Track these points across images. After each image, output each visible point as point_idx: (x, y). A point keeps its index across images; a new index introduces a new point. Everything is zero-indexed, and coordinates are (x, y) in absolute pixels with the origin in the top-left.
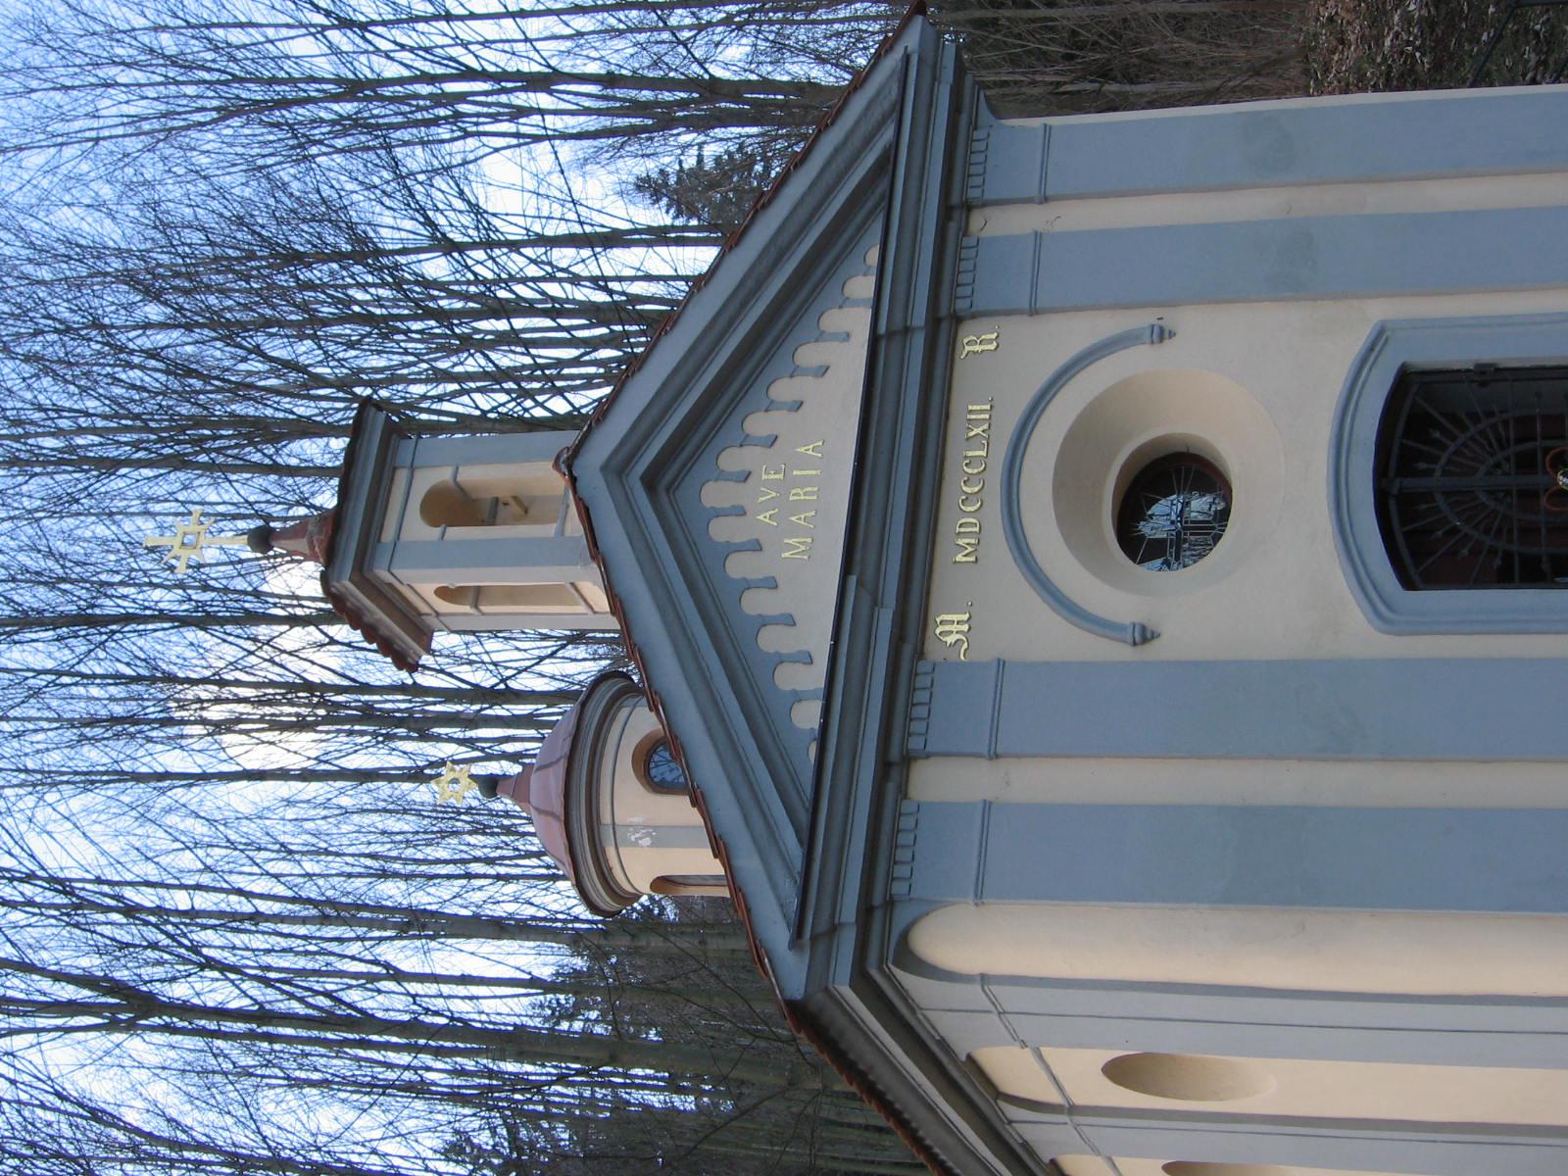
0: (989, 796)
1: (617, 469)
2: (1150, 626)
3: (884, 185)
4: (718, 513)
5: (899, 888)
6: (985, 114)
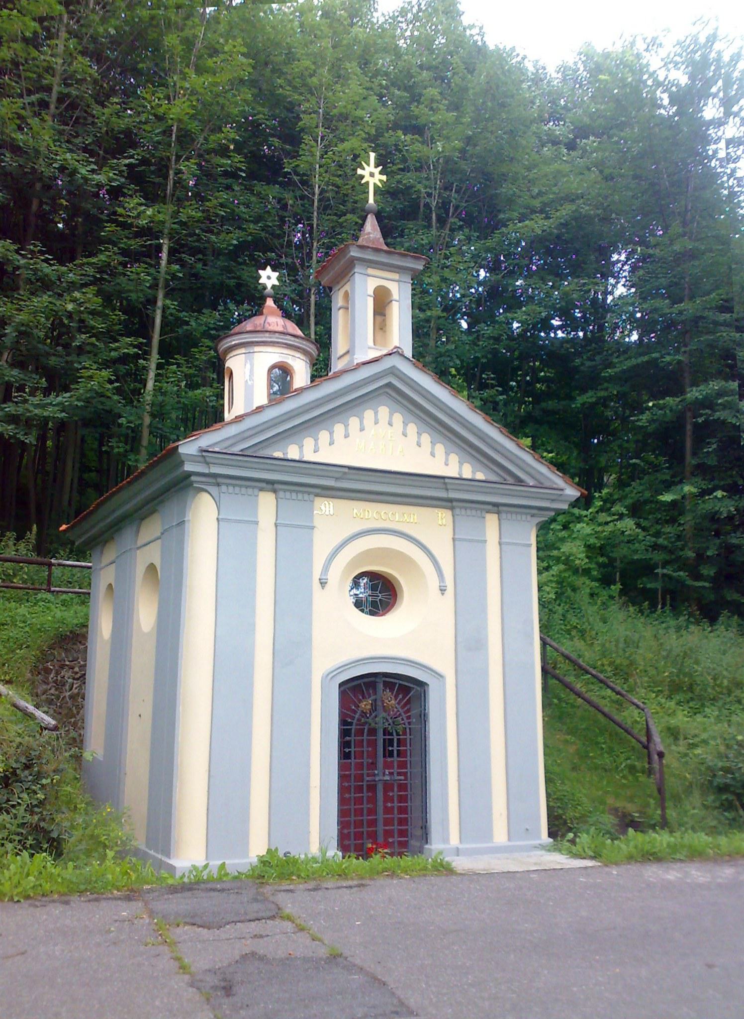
1: (393, 371)
2: (327, 585)
3: (510, 480)
4: (376, 413)
5: (224, 488)
6: (178, 874)
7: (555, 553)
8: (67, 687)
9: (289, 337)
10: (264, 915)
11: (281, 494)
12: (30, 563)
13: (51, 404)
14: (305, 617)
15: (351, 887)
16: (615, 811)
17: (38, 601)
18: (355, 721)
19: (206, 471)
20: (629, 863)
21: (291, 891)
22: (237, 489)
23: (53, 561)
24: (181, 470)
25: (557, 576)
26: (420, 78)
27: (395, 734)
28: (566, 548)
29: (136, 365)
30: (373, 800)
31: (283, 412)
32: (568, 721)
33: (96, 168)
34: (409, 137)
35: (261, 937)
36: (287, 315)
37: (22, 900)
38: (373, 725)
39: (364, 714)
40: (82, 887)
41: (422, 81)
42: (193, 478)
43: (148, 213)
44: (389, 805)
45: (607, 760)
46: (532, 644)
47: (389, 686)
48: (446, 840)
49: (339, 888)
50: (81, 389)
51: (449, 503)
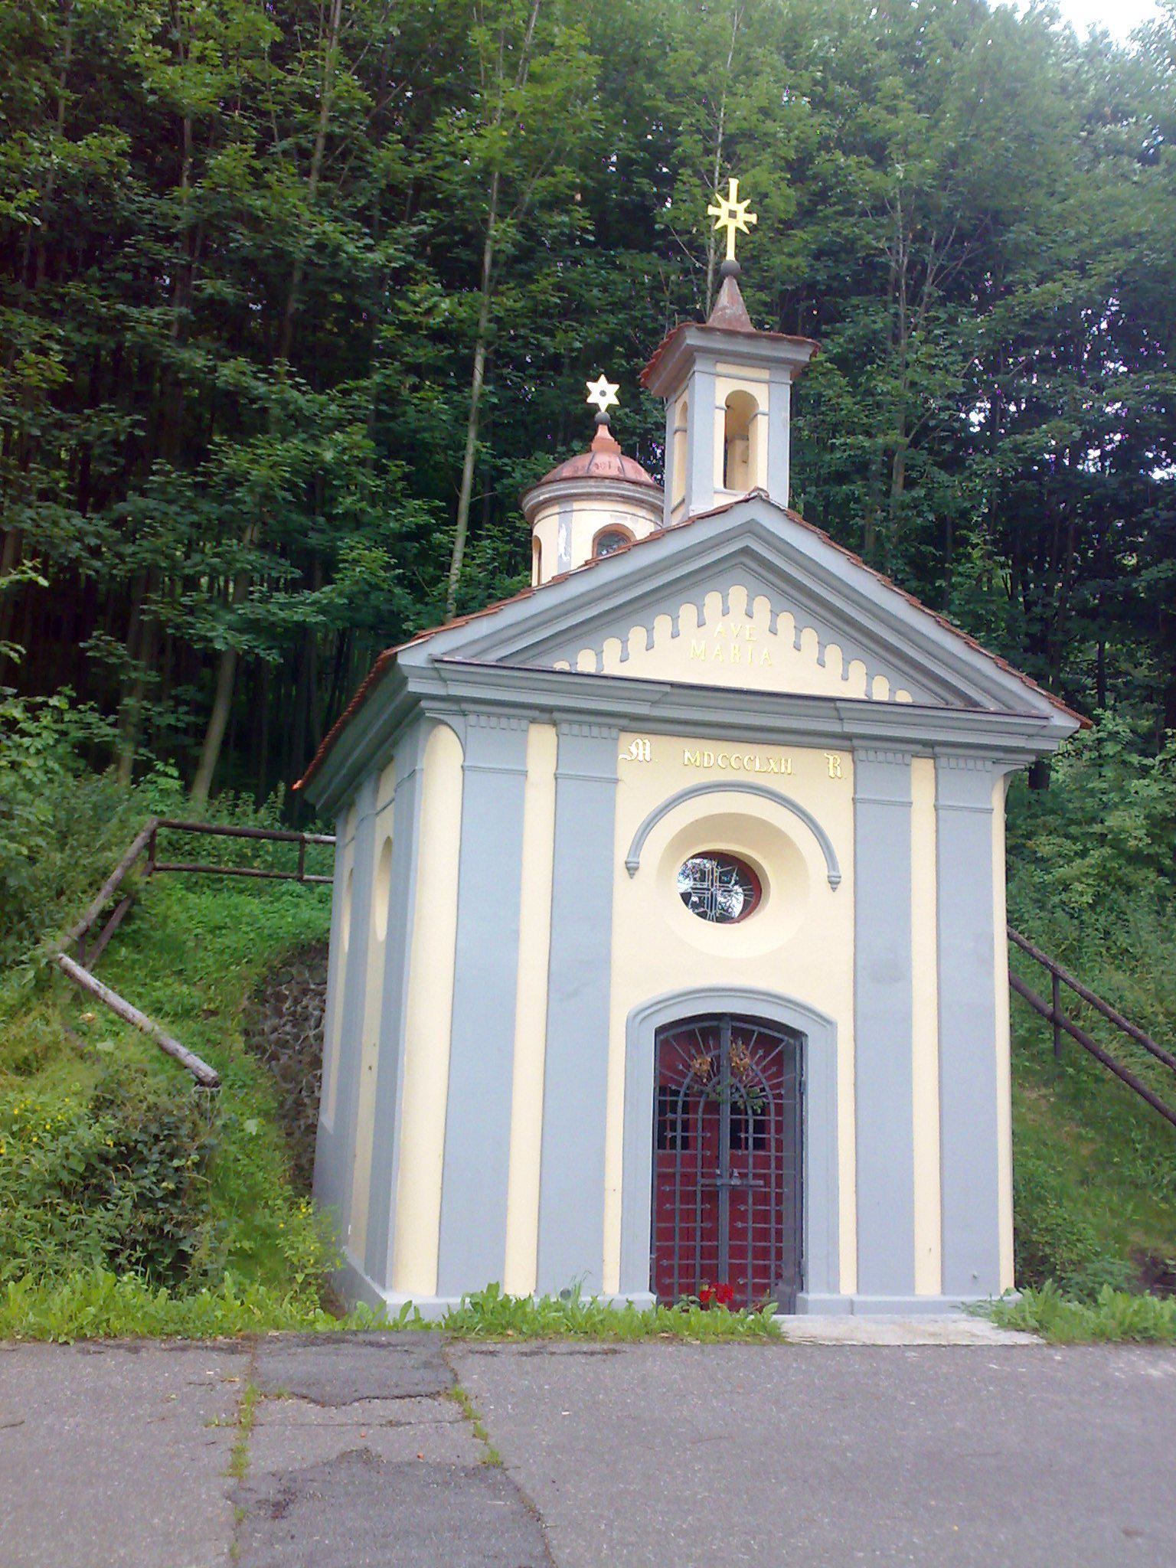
0: (530, 774)
1: (751, 528)
3: (959, 704)
5: (472, 719)
7: (1097, 828)
8: (312, 1022)
9: (627, 485)
10: (419, 1389)
11: (565, 728)
12: (275, 838)
13: (303, 603)
14: (601, 919)
15: (592, 1353)
16: (1139, 1255)
17: (283, 894)
18: (682, 1091)
19: (442, 692)
20: (1095, 1344)
21: (492, 1353)
22: (494, 721)
23: (307, 835)
24: (404, 693)
25: (1097, 866)
26: (877, 62)
27: (750, 1112)
28: (1113, 820)
29: (429, 541)
30: (712, 1215)
31: (565, 598)
32: (1087, 1103)
33: (371, 242)
34: (853, 160)
35: (399, 1424)
36: (628, 452)
37: (72, 1343)
38: (713, 1096)
39: (697, 1078)
40: (171, 1328)
41: (881, 67)
42: (424, 704)
43: (443, 306)
44: (739, 1225)
45: (1141, 1170)
46: (990, 973)
47: (737, 1033)
48: (834, 1287)
49: (571, 1354)
50: (348, 580)
51: (845, 742)
